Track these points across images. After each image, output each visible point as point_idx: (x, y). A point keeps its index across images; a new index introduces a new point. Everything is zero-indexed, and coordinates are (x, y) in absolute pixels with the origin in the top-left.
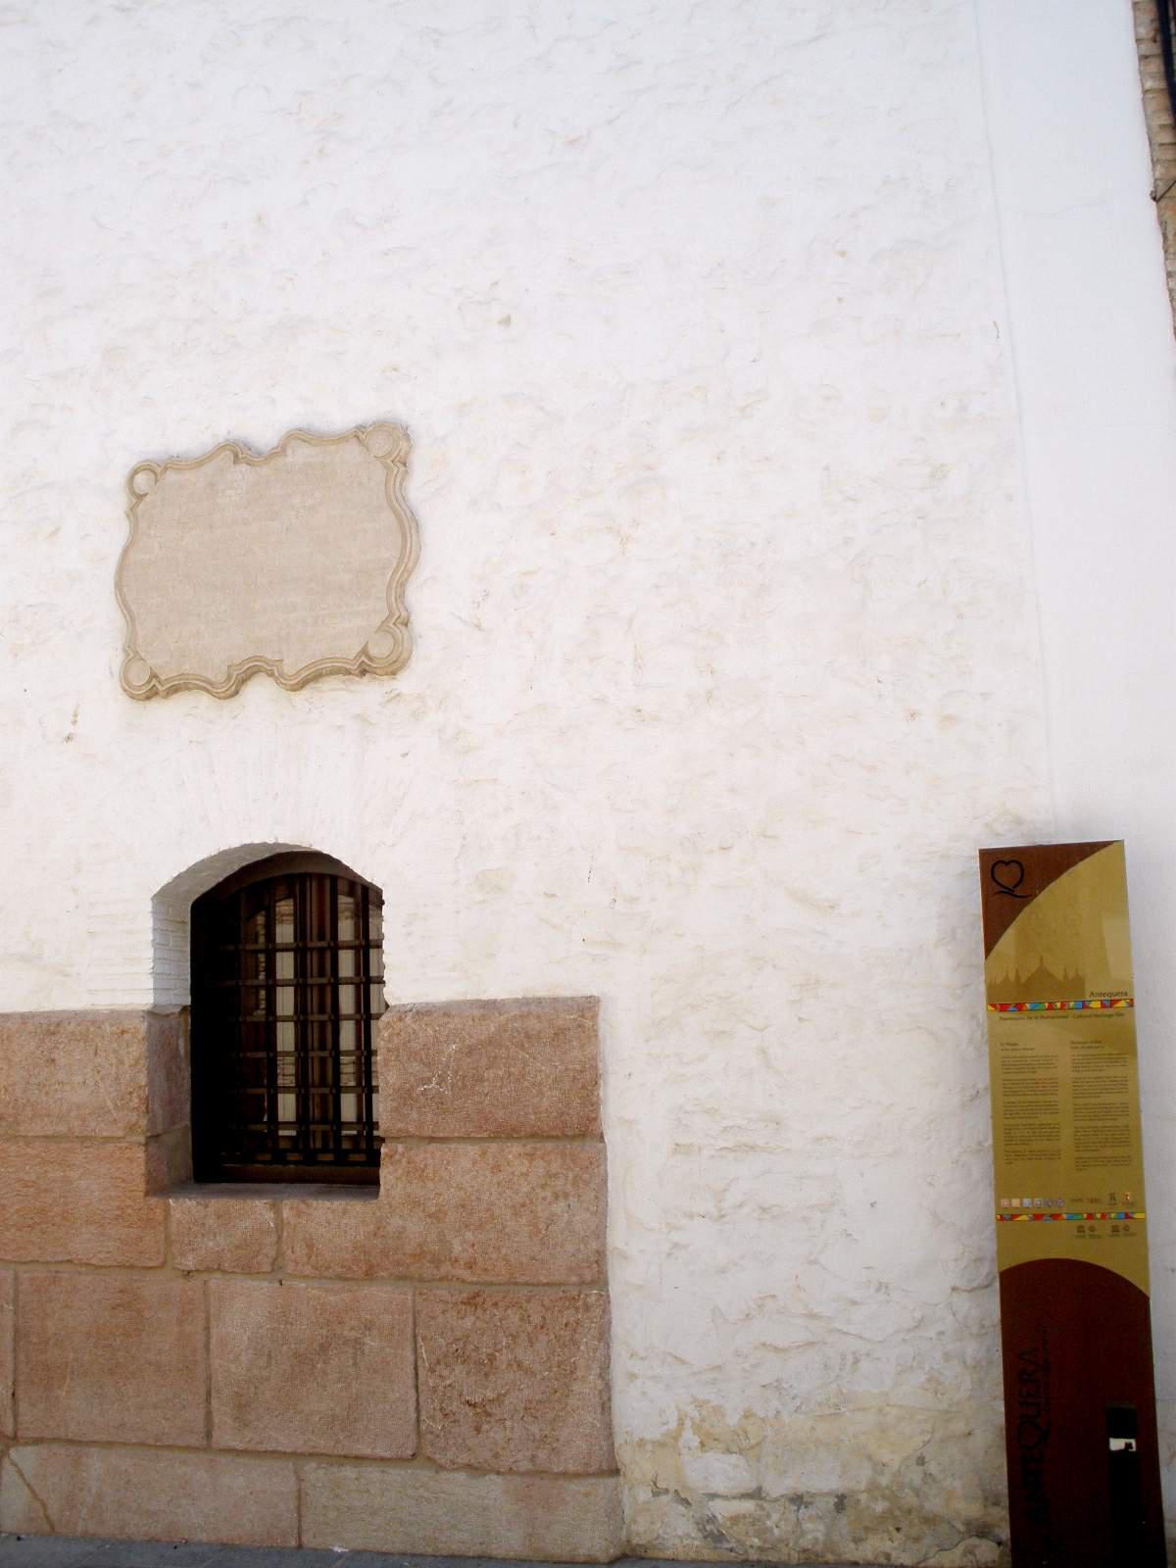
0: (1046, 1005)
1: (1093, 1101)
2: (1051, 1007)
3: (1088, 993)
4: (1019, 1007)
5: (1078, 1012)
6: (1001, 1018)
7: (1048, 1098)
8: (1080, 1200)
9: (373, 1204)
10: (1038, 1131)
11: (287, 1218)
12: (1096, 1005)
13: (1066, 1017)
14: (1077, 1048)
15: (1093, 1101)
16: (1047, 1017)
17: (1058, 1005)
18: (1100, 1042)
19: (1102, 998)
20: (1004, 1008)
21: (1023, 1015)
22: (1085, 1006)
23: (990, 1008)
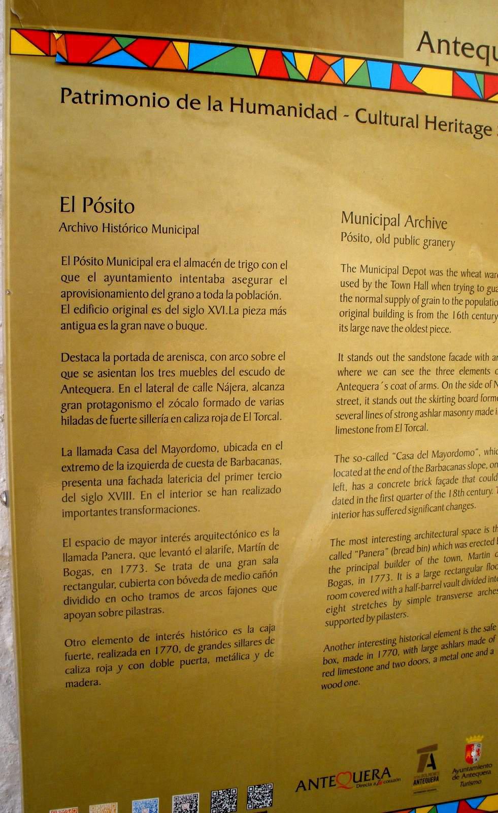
0: (258, 56)
1: (408, 443)
2: (276, 68)
3: (411, 39)
4: (150, 54)
5: (373, 102)
6: (65, 91)
7: (240, 433)
8: (331, 781)
9: (417, 749)
10: (195, 560)
11: (9, 635)
12: (436, 82)
13: (331, 114)
14: (361, 239)
15: (408, 443)
16: (259, 108)
17: (304, 63)
18: (442, 225)
19: (460, 62)
20: (82, 51)
21: (172, 86)
22: (401, 85)
23: (22, 45)
